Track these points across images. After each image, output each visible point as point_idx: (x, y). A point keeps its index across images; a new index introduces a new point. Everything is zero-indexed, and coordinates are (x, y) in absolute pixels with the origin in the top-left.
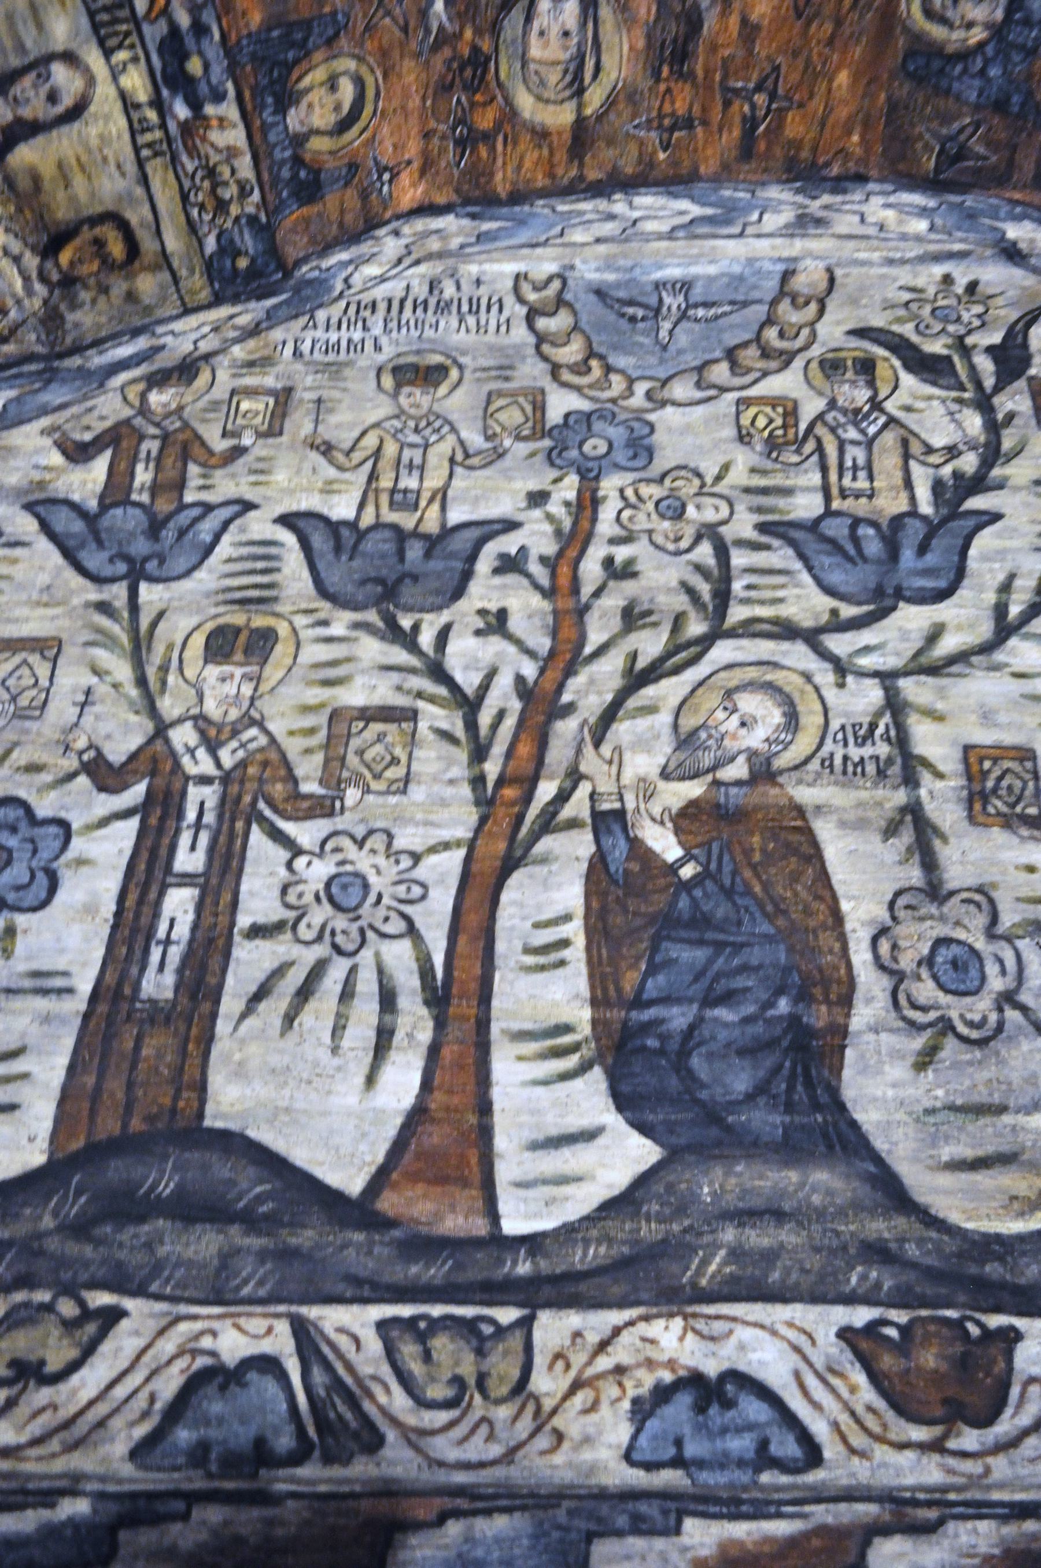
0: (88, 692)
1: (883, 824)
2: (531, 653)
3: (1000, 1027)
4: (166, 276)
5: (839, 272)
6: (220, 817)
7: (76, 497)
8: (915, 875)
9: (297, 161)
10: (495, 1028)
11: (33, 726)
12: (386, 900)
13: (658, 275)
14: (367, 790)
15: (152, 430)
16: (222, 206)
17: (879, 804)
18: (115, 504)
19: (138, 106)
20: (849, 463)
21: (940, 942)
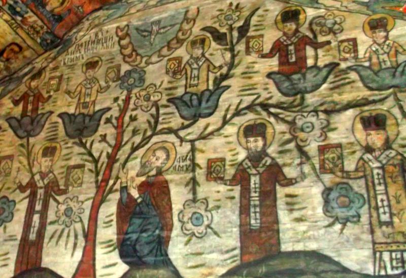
0: (19, 168)
1: (185, 183)
2: (110, 146)
3: (206, 233)
4: (31, 50)
5: (201, 8)
6: (44, 196)
7: (16, 116)
8: (191, 196)
9: (53, 15)
10: (97, 241)
11: (8, 178)
12: (76, 214)
13: (152, 20)
14: (73, 187)
15: (32, 94)
16: (38, 32)
17: (185, 178)
18: (25, 117)
19: (9, 21)
20: (193, 76)
21: (195, 213)
